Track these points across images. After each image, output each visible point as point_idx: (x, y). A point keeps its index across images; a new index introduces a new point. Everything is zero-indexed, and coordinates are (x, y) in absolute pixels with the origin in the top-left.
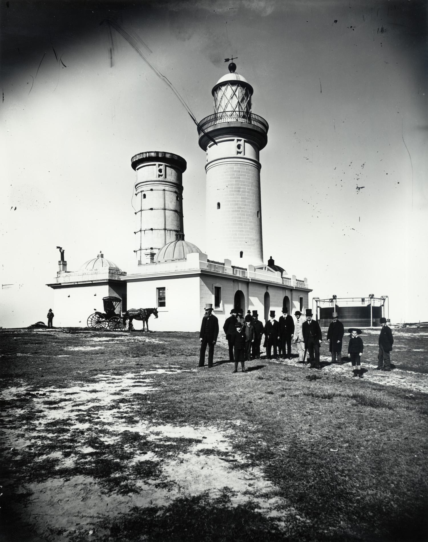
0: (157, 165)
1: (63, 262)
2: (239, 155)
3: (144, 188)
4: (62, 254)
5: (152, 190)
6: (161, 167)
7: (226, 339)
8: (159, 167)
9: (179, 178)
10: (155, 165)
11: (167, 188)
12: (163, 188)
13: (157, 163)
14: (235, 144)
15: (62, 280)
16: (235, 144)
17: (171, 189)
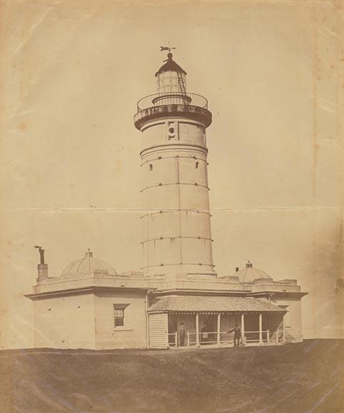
0: (167, 123)
1: (43, 266)
2: (172, 141)
3: (150, 157)
4: (42, 252)
5: (160, 158)
6: (172, 126)
7: (300, 300)
8: (169, 125)
9: (202, 139)
10: (164, 123)
11: (181, 154)
12: (177, 154)
13: (166, 121)
14: (166, 128)
15: (43, 290)
16: (166, 128)
17: (186, 154)
